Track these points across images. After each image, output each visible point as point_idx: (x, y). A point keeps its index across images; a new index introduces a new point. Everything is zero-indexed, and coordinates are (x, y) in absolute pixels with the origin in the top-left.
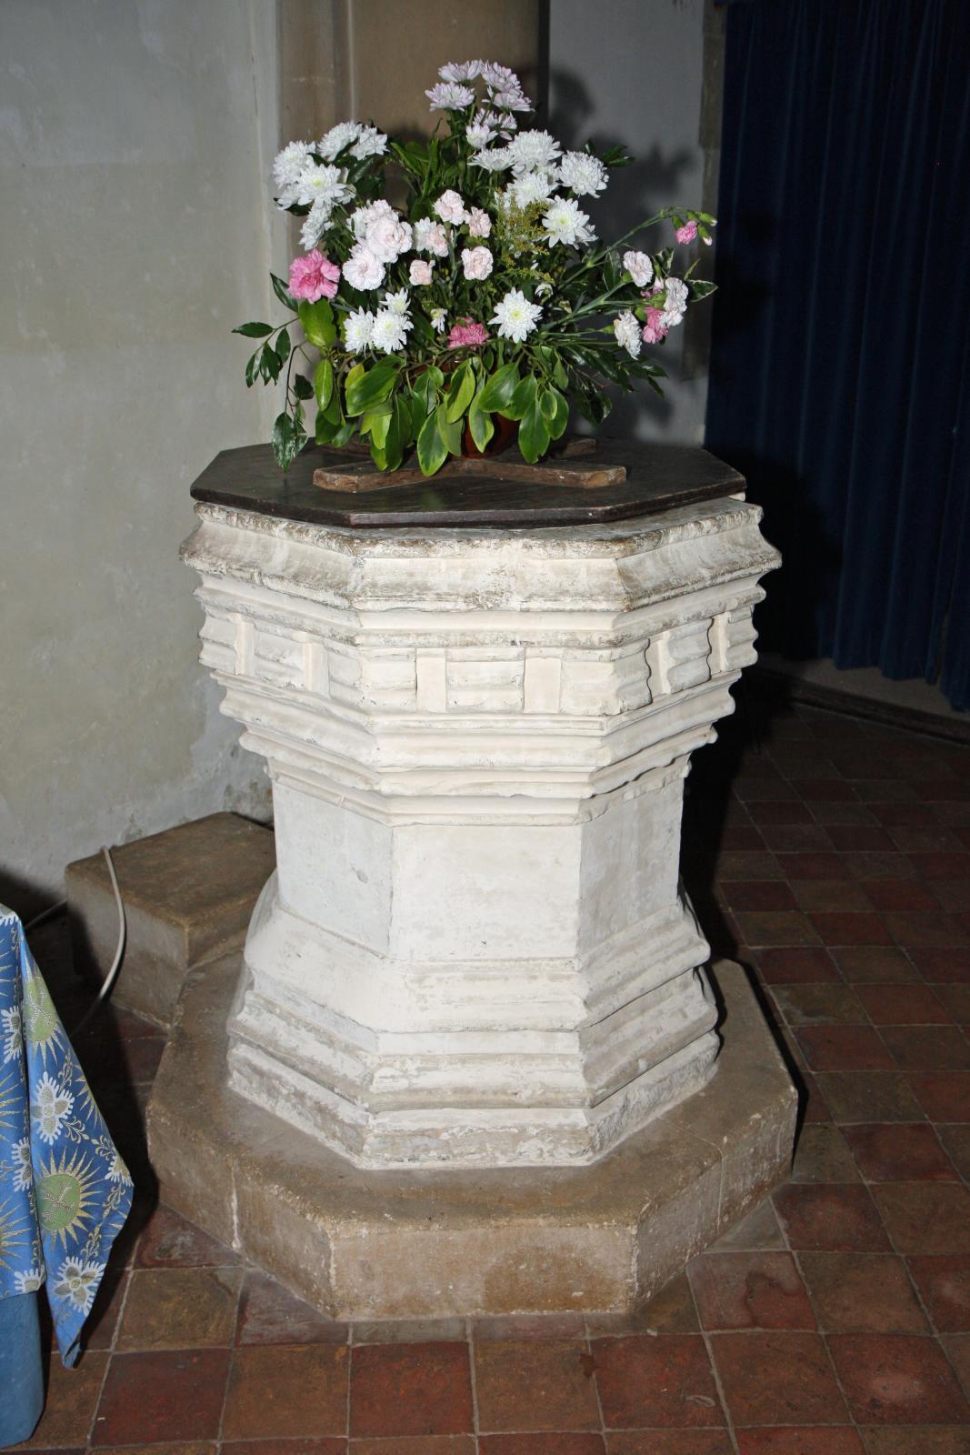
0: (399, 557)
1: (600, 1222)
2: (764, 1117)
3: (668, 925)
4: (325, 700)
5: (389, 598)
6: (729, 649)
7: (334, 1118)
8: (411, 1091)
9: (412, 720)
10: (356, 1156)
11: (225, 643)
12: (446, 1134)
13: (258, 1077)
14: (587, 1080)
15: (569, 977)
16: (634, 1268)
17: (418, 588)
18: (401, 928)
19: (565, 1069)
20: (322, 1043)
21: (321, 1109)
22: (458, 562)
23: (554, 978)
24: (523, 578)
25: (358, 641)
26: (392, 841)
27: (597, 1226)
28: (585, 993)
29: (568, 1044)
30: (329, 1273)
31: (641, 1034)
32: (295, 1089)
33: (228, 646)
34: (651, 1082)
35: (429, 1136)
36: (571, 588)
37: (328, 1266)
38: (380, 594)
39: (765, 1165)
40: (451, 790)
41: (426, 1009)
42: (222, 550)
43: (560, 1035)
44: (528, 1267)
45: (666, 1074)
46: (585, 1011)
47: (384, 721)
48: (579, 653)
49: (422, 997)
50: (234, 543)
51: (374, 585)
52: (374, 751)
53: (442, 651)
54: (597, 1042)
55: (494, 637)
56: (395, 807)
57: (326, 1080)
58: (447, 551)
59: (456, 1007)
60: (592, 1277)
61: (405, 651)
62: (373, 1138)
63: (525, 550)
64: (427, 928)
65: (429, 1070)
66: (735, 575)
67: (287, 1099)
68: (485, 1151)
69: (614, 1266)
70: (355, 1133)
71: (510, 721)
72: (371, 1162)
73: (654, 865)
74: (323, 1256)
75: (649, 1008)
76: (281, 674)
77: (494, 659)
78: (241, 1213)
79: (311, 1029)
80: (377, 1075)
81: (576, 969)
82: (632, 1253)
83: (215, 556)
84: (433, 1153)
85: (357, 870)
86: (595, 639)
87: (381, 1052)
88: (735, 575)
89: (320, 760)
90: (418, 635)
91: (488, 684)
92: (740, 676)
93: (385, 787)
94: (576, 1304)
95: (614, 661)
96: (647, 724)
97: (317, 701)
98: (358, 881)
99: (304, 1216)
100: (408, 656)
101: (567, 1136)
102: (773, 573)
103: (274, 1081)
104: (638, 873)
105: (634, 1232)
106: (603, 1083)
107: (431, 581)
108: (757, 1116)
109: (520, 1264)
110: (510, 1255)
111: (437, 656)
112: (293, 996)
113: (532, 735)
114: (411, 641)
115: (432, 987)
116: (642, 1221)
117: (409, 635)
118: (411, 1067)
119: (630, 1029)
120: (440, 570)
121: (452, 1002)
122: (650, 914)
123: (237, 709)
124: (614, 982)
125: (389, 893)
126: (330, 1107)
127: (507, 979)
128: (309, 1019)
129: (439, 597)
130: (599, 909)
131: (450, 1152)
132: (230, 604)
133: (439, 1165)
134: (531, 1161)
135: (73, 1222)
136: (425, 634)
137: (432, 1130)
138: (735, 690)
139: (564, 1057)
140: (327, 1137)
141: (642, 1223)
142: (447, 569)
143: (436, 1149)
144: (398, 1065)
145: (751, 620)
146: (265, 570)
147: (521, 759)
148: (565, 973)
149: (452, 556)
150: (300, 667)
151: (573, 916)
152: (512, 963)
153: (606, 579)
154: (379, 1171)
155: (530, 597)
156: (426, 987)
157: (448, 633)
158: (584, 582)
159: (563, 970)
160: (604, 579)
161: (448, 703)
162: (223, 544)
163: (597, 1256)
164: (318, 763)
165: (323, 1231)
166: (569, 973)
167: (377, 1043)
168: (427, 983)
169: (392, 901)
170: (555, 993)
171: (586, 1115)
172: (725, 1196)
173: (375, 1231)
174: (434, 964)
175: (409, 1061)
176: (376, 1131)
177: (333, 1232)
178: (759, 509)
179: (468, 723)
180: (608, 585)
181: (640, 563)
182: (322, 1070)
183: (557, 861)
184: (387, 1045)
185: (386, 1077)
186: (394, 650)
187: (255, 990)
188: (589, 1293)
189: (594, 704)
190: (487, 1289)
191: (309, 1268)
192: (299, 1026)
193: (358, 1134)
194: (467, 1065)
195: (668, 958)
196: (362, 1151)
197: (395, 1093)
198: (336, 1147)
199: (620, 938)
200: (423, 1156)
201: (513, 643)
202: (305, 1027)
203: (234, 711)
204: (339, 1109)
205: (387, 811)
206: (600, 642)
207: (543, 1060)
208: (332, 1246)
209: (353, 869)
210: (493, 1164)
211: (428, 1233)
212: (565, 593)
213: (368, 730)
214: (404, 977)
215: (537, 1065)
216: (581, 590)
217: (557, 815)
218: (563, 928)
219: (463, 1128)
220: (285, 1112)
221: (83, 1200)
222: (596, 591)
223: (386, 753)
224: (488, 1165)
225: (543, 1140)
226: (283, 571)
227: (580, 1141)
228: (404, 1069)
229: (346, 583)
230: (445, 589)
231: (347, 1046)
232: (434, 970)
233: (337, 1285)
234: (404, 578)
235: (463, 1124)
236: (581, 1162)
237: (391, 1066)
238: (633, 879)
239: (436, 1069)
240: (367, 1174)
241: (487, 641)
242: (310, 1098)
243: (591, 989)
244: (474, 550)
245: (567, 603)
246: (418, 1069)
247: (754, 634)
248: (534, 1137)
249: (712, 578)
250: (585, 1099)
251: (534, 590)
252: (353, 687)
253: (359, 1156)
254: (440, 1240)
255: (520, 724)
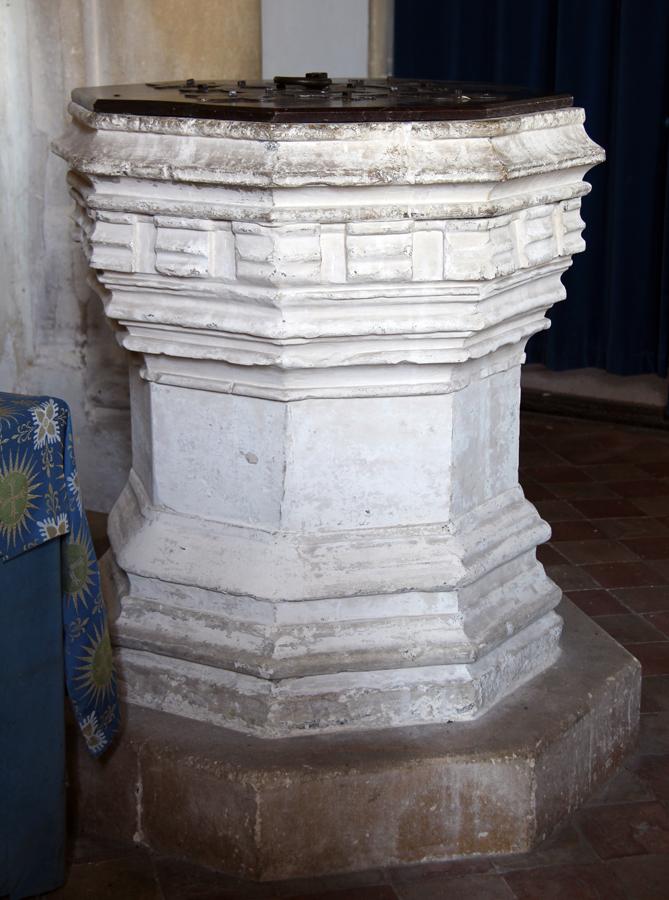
0: (309, 140)
1: (502, 756)
2: (617, 680)
3: (513, 506)
4: (229, 282)
5: (303, 174)
6: (565, 234)
7: (234, 695)
8: (310, 655)
9: (315, 292)
10: (259, 728)
11: (121, 242)
12: (344, 697)
13: (142, 677)
14: (468, 636)
15: (445, 540)
16: (533, 804)
17: (327, 165)
18: (294, 501)
19: (447, 627)
20: (213, 627)
21: (217, 690)
22: (358, 144)
23: (432, 542)
24: (413, 156)
25: (273, 216)
26: (286, 417)
27: (499, 760)
28: (462, 553)
29: (447, 603)
30: (253, 830)
31: (503, 603)
32: (187, 678)
33: (124, 246)
34: (514, 648)
35: (329, 700)
36: (456, 163)
37: (253, 823)
38: (296, 171)
39: (621, 730)
40: (344, 361)
41: (321, 576)
42: (123, 153)
43: (441, 595)
44: (438, 808)
45: (526, 643)
46: (463, 569)
47: (290, 294)
48: (459, 223)
49: (316, 566)
50: (135, 146)
51: (289, 164)
52: (280, 324)
53: (343, 226)
54: (472, 605)
55: (389, 210)
56: (291, 382)
57: (223, 660)
58: (350, 133)
59: (347, 572)
60: (496, 815)
61: (312, 226)
62: (277, 706)
63: (414, 132)
64: (317, 500)
65: (324, 636)
66: (574, 162)
67: (177, 690)
68: (381, 712)
69: (515, 802)
70: (258, 704)
71: (399, 290)
72: (275, 730)
73: (501, 445)
74: (247, 814)
75: (507, 581)
76: (183, 264)
77: (389, 232)
78: (146, 801)
79: (199, 617)
80: (277, 644)
81: (452, 531)
82: (531, 788)
83: (117, 158)
84: (332, 718)
85: (245, 453)
86: (476, 210)
87: (280, 621)
88: (574, 162)
89: (215, 347)
90: (325, 210)
91: (383, 254)
92: (571, 263)
93: (286, 359)
94: (483, 845)
95: (489, 230)
96: (506, 298)
97: (220, 285)
98: (248, 464)
99: (226, 777)
100: (315, 231)
101: (455, 691)
102: (557, 305)
103: (161, 676)
104: (491, 451)
105: (532, 765)
106: (482, 639)
107: (337, 160)
108: (611, 679)
109: (431, 806)
110: (422, 797)
111: (337, 231)
112: (178, 590)
113: (406, 304)
114: (318, 216)
115: (323, 556)
116: (538, 755)
117: (316, 211)
118: (308, 634)
119: (494, 598)
120: (343, 151)
121: (344, 568)
122: (500, 493)
123: (126, 309)
124: (481, 547)
125: (282, 468)
126: (228, 686)
127: (390, 545)
128: (196, 610)
129: (347, 173)
130: (464, 471)
131: (348, 715)
132: (131, 203)
133: (339, 728)
134: (422, 720)
135: (94, 652)
136: (331, 210)
137: (331, 693)
138: (567, 278)
139: (445, 617)
140: (225, 718)
141: (538, 756)
142: (350, 150)
143: (335, 713)
144: (296, 632)
145: (579, 211)
146: (174, 163)
147: (406, 326)
148: (441, 537)
149: (354, 138)
150: (206, 254)
151: (445, 482)
152: (394, 530)
153: (484, 155)
154: (283, 739)
155: (423, 171)
156: (317, 556)
157: (350, 209)
158: (465, 158)
159: (439, 534)
160: (481, 155)
161: (348, 273)
162: (122, 148)
163: (500, 792)
164: (213, 350)
165: (248, 785)
166: (446, 536)
167: (275, 613)
168: (317, 552)
169: (285, 475)
170: (435, 555)
171: (469, 670)
172: (594, 753)
173: (297, 781)
174: (324, 534)
175: (306, 629)
176: (279, 698)
177: (258, 784)
178: (582, 111)
179: (364, 291)
180: (486, 160)
181: (506, 144)
182: (218, 651)
183: (431, 430)
184: (287, 614)
185: (286, 645)
186: (303, 226)
187: (132, 595)
188: (493, 833)
189: (475, 269)
190: (401, 835)
191: (230, 833)
192: (187, 617)
193: (262, 703)
194: (359, 629)
195: (519, 532)
196: (266, 720)
197: (297, 658)
198: (236, 725)
199: (480, 510)
200: (323, 721)
201: (406, 215)
202: (193, 616)
203: (123, 312)
204: (237, 686)
205: (281, 387)
206: (480, 212)
207: (427, 620)
208: (258, 799)
209: (242, 453)
210: (387, 725)
211: (347, 778)
212: (451, 167)
213: (277, 305)
214: (297, 549)
215: (422, 625)
216: (465, 164)
217: (433, 384)
218: (437, 494)
219: (359, 689)
220: (176, 705)
221: (87, 671)
222: (476, 164)
223: (289, 324)
224: (383, 726)
225: (433, 696)
226: (194, 163)
227: (466, 695)
228: (302, 636)
229: (263, 164)
230: (350, 166)
231: (242, 624)
232: (325, 540)
233: (262, 841)
234: (314, 158)
235: (358, 686)
236: (467, 717)
237: (289, 634)
238: (487, 456)
239: (332, 635)
240: (274, 742)
241: (384, 214)
242: (204, 682)
243: (466, 551)
244: (373, 132)
245: (455, 177)
246: (315, 636)
247: (583, 224)
248: (424, 694)
249: (560, 162)
250: (469, 652)
251: (424, 165)
252: (266, 262)
253: (262, 726)
254: (358, 786)
255: (409, 290)
